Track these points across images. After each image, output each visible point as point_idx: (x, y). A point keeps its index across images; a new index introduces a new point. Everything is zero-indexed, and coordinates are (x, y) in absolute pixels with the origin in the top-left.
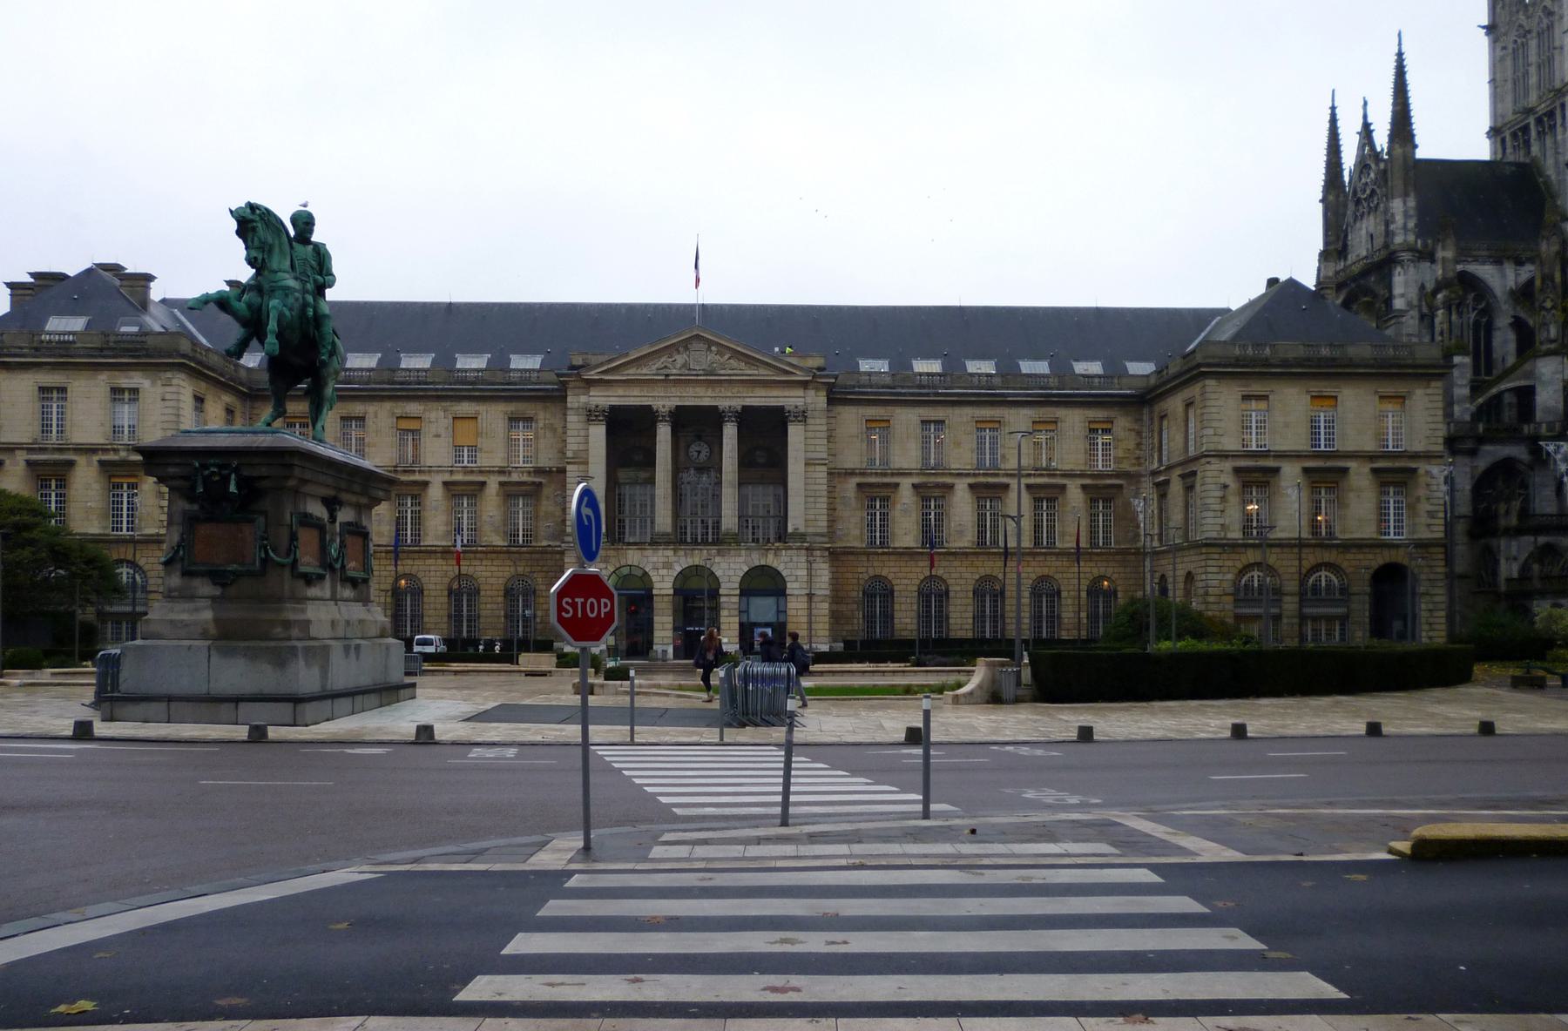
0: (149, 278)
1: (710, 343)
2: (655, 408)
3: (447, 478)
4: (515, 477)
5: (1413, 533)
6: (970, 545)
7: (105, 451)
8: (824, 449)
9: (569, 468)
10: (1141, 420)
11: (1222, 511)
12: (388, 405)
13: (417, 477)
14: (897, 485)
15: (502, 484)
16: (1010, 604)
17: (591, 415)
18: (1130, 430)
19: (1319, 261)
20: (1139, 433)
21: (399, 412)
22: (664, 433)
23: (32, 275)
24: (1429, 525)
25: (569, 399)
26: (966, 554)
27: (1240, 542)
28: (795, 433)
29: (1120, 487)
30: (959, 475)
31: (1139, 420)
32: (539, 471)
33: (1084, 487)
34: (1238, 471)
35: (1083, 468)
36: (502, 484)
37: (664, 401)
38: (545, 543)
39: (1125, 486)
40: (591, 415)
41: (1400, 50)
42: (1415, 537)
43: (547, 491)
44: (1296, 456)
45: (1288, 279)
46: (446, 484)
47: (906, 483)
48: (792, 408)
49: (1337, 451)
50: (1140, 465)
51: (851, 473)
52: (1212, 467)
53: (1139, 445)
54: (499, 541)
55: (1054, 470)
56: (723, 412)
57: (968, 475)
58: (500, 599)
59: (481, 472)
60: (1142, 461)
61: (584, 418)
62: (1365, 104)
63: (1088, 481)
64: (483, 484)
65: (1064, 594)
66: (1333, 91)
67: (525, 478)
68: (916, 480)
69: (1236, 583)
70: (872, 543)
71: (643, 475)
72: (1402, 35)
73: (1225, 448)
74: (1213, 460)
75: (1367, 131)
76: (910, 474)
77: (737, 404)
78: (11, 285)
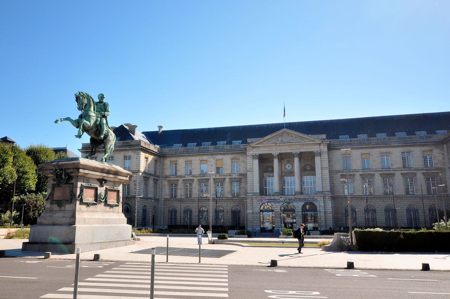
0: (133, 128)
2: (273, 154)
3: (214, 177)
4: (234, 176)
8: (328, 164)
9: (248, 173)
12: (198, 157)
13: (206, 178)
14: (354, 175)
17: (254, 157)
20: (443, 154)
21: (201, 159)
22: (276, 161)
25: (247, 153)
26: (402, 197)
28: (317, 159)
31: (443, 149)
32: (241, 175)
33: (423, 173)
37: (275, 151)
38: (243, 196)
40: (254, 157)
43: (243, 181)
47: (357, 174)
48: (316, 152)
50: (445, 165)
51: (339, 172)
54: (229, 196)
61: (252, 158)
63: (425, 171)
65: (419, 211)
67: (236, 177)
68: (361, 173)
70: (172, 197)
71: (271, 175)
77: (298, 151)
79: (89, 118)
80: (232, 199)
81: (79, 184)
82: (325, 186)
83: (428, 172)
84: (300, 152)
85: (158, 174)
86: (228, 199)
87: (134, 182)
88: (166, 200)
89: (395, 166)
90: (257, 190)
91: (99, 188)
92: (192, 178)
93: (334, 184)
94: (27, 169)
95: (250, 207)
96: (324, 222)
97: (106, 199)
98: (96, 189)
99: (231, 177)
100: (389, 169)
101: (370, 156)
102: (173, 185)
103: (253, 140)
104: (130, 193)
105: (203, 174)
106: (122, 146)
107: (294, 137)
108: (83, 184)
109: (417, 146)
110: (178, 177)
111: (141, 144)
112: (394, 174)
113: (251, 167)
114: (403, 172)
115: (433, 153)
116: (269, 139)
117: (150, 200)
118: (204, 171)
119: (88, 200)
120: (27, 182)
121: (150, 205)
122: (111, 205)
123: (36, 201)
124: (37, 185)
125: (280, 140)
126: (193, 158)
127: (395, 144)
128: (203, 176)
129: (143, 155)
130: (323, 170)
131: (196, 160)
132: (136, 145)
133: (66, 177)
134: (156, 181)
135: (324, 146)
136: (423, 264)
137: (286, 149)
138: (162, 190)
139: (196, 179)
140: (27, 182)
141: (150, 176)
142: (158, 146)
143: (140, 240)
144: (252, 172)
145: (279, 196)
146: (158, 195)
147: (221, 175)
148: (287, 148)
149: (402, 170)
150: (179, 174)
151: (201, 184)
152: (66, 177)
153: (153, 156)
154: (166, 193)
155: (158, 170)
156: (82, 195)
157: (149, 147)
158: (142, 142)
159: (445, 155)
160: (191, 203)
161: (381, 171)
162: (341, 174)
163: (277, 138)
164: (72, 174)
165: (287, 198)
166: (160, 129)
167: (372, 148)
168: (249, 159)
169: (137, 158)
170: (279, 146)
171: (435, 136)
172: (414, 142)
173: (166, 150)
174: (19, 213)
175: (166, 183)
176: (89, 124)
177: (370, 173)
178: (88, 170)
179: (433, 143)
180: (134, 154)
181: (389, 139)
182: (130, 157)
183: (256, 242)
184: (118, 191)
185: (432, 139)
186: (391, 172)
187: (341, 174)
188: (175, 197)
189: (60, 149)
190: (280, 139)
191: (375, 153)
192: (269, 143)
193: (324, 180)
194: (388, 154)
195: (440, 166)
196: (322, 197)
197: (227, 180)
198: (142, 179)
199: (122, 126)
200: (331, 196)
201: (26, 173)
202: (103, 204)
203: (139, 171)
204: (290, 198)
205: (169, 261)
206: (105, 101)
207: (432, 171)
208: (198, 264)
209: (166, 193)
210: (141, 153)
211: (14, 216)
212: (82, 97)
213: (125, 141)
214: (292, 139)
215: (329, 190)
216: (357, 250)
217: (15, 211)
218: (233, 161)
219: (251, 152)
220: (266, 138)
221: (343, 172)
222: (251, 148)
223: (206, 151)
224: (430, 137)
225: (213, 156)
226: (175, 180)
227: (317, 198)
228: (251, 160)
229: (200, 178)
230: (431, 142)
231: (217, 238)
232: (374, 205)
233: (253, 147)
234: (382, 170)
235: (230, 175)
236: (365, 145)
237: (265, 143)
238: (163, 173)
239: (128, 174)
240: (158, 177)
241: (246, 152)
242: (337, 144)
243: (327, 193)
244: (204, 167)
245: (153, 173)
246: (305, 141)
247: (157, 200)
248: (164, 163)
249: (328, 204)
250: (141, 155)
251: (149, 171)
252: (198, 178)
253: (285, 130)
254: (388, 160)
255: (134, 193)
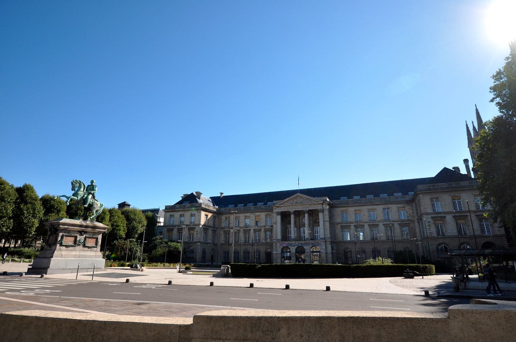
0: (199, 194)
1: (301, 197)
2: (290, 211)
3: (254, 228)
5: (494, 233)
6: (370, 240)
7: (189, 226)
10: (413, 206)
11: (429, 229)
13: (248, 228)
14: (350, 226)
15: (264, 229)
16: (251, 254)
17: (278, 214)
18: (410, 209)
19: (464, 162)
20: (413, 210)
23: (184, 195)
24: (499, 230)
25: (274, 211)
27: (436, 237)
28: (321, 215)
29: (409, 223)
30: (366, 222)
31: (412, 206)
33: (399, 224)
34: (432, 217)
35: (398, 219)
36: (264, 229)
37: (292, 209)
39: (411, 223)
40: (278, 214)
41: (476, 108)
42: (495, 234)
44: (450, 213)
45: (444, 168)
46: (254, 229)
47: (352, 225)
48: (319, 209)
49: (463, 211)
50: (414, 218)
51: (339, 223)
52: (425, 217)
53: (413, 213)
55: (390, 220)
56: (305, 211)
57: (368, 222)
58: (264, 254)
59: (260, 227)
60: (415, 217)
62: (473, 122)
63: (400, 223)
64: (261, 229)
66: (466, 121)
67: (269, 228)
68: (355, 224)
69: (437, 248)
70: (246, 242)
72: (476, 105)
73: (428, 212)
74: (424, 215)
75: (474, 128)
76: (353, 223)
77: (307, 209)
78: (220, 193)
79: (77, 195)
80: (266, 244)
81: (61, 234)
82: (326, 234)
83: (402, 223)
84: (309, 210)
85: (216, 226)
86: (263, 244)
87: (197, 232)
88: (222, 244)
89: (379, 219)
90: (279, 237)
91: (78, 236)
92: (239, 229)
93: (336, 232)
94: (119, 224)
95: (275, 249)
96: (325, 260)
97: (84, 243)
98: (76, 237)
99: (265, 228)
100: (375, 221)
101: (361, 212)
102: (227, 233)
103: (278, 201)
104: (194, 239)
105: (246, 226)
106: (190, 207)
107: (305, 199)
108: (64, 234)
109: (393, 204)
110: (230, 228)
111: (202, 206)
112: (378, 225)
113: (276, 220)
114: (384, 223)
115: (406, 209)
116: (288, 201)
117: (209, 244)
118: (248, 224)
119: (68, 243)
120: (118, 232)
121: (242, 249)
122: (89, 247)
123: (124, 245)
124: (127, 234)
125: (295, 201)
126: (240, 215)
127: (378, 203)
128: (246, 227)
129: (203, 213)
130: (325, 223)
131: (242, 216)
132: (199, 206)
133: (54, 230)
134: (214, 231)
135: (325, 205)
136: (286, 285)
137: (299, 208)
138: (219, 237)
139: (242, 230)
140: (118, 232)
141: (209, 228)
142: (217, 207)
143: (144, 270)
144: (275, 224)
145: (294, 242)
146: (216, 241)
147: (259, 227)
148: (300, 207)
149: (384, 222)
150: (231, 226)
151: (267, 232)
152: (54, 230)
153: (212, 214)
154: (222, 239)
155: (217, 224)
156: (62, 240)
157: (209, 207)
158: (202, 204)
159: (414, 210)
160: (238, 246)
161: (369, 222)
162: (341, 225)
163: (293, 200)
164: (58, 228)
165: (300, 243)
166: (221, 195)
167: (362, 206)
168: (275, 215)
169: (199, 216)
170: (294, 205)
171: (407, 196)
172: (391, 201)
173: (223, 209)
174: (110, 253)
175: (222, 232)
176: (77, 199)
177: (361, 224)
178: (67, 226)
179: (405, 202)
180: (197, 213)
181: (374, 199)
182: (194, 214)
183: (206, 272)
184: (97, 239)
185: (405, 198)
186: (376, 223)
187: (341, 225)
188: (248, 242)
189: (146, 210)
190: (295, 201)
191: (379, 209)
192: (288, 204)
193: (326, 230)
194: (373, 210)
195: (411, 219)
196: (324, 242)
197: (263, 230)
198: (203, 230)
199: (192, 193)
200: (331, 241)
201: (118, 226)
202: (81, 246)
203: (200, 224)
204: (302, 243)
205: (77, 279)
206: (94, 184)
207: (406, 222)
208: (75, 280)
209: (222, 239)
210: (202, 212)
211: (107, 255)
212: (75, 183)
213: (192, 204)
214: (303, 201)
215: (329, 237)
216: (231, 277)
217: (108, 251)
218: (267, 216)
219: (276, 210)
220: (285, 200)
221: (342, 224)
222: (276, 207)
223: (249, 210)
224: (403, 197)
225: (254, 213)
226: (228, 230)
227: (321, 243)
228: (276, 216)
229: (244, 229)
230: (403, 201)
231: (184, 269)
232: (364, 248)
233: (277, 207)
234: (370, 222)
235: (264, 227)
236: (357, 204)
237: (286, 203)
238: (220, 225)
239: (106, 228)
240: (217, 228)
241: (273, 211)
242: (338, 204)
243: (328, 239)
244: (248, 221)
245: (212, 226)
246: (312, 202)
247: (215, 245)
248: (221, 218)
249: (329, 247)
250: (201, 213)
251: (208, 224)
252: (243, 229)
253: (298, 194)
254: (374, 214)
255: (196, 239)
